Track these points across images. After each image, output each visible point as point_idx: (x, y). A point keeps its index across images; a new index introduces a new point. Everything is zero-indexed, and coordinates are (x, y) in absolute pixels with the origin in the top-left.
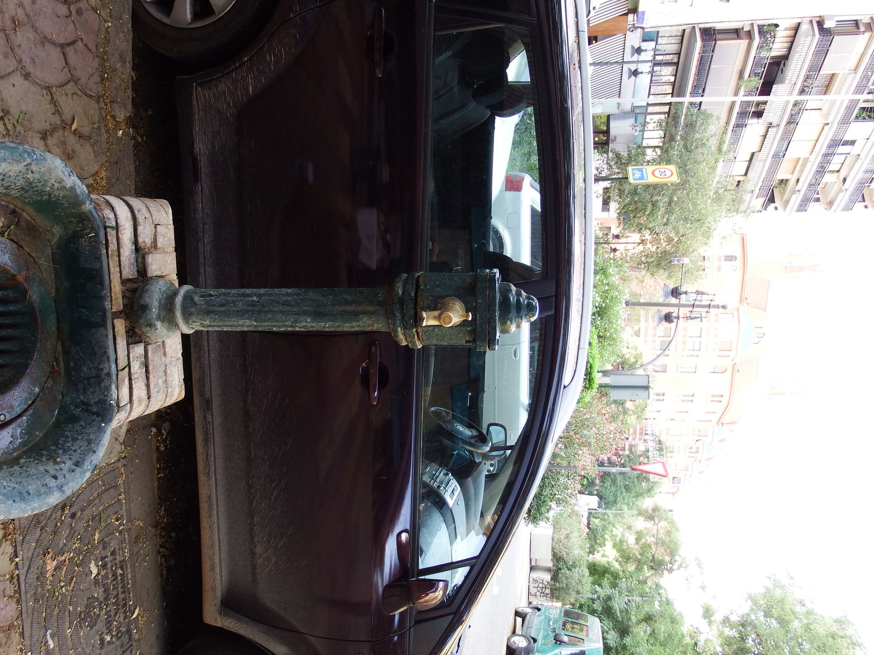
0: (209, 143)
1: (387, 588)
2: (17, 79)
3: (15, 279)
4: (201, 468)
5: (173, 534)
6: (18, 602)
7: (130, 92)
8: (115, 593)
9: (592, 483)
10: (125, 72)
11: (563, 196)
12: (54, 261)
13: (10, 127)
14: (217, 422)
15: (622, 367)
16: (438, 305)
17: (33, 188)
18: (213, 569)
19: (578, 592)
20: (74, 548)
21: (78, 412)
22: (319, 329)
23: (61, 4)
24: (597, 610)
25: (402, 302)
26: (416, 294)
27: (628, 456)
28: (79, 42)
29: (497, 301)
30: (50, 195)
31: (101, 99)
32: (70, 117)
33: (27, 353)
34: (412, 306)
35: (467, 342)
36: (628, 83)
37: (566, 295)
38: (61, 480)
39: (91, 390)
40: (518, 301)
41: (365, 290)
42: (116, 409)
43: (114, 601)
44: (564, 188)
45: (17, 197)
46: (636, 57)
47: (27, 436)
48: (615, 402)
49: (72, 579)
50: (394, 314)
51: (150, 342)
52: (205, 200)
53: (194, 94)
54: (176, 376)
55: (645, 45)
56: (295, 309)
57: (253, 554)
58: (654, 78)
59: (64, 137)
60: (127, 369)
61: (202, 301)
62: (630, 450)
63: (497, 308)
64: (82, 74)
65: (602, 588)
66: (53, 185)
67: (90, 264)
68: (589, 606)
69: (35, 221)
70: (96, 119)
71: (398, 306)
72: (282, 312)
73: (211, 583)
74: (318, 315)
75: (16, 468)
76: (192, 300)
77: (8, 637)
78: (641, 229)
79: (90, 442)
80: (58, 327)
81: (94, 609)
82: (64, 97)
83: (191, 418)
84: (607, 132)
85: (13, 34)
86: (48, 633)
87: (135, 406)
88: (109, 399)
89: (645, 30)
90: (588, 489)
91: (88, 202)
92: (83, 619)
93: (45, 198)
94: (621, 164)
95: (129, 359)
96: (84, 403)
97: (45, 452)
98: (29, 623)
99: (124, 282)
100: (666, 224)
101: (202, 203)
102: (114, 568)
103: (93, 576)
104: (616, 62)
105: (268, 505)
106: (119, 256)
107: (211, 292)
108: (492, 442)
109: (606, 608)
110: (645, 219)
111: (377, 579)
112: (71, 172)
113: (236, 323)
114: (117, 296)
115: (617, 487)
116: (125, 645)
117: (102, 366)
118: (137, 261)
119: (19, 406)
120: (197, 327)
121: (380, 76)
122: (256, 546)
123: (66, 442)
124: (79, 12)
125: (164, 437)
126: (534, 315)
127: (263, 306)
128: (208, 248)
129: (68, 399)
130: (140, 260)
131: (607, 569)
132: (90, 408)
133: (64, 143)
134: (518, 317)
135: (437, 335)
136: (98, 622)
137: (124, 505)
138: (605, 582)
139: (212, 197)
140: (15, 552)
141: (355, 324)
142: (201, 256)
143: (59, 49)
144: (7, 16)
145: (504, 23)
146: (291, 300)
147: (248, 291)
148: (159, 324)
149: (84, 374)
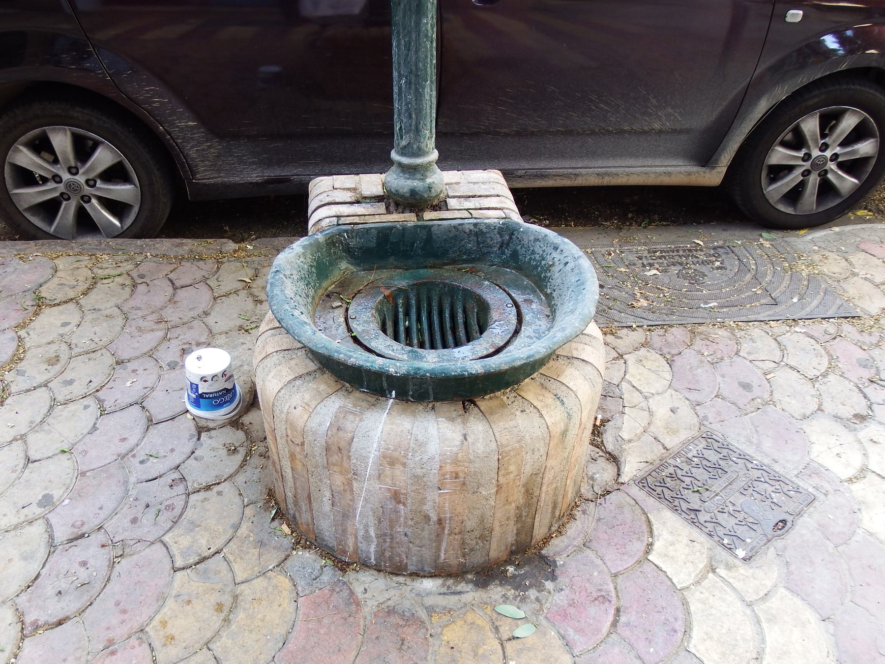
0: (251, 167)
2: (210, 320)
3: (388, 296)
4: (569, 182)
5: (630, 215)
6: (671, 326)
8: (677, 258)
10: (189, 245)
12: (371, 269)
14: (525, 165)
20: (630, 287)
21: (508, 252)
22: (434, 10)
23: (137, 289)
30: (311, 266)
32: (240, 283)
33: (453, 291)
38: (568, 259)
39: (489, 241)
45: (315, 292)
49: (659, 289)
53: (204, 181)
54: (479, 175)
56: (414, 36)
57: (660, 132)
60: (470, 211)
61: (406, 137)
64: (199, 275)
66: (302, 262)
67: (372, 238)
72: (417, 51)
73: (682, 176)
75: (554, 295)
76: (405, 147)
77: (700, 333)
79: (537, 240)
80: (431, 267)
85: (171, 323)
87: (505, 206)
88: (499, 225)
92: (696, 282)
93: (313, 269)
95: (461, 210)
96: (501, 247)
98: (692, 319)
99: (388, 211)
101: (310, 175)
103: (658, 273)
105: (613, 114)
106: (365, 215)
107: (398, 129)
113: (428, 103)
114: (402, 217)
117: (467, 231)
120: (431, 143)
122: (653, 129)
123: (535, 260)
124: (142, 276)
127: (411, 72)
137: (596, 249)
139: (303, 165)
140: (627, 327)
143: (178, 291)
144: (155, 327)
147: (396, 89)
148: (429, 181)
149: (474, 246)
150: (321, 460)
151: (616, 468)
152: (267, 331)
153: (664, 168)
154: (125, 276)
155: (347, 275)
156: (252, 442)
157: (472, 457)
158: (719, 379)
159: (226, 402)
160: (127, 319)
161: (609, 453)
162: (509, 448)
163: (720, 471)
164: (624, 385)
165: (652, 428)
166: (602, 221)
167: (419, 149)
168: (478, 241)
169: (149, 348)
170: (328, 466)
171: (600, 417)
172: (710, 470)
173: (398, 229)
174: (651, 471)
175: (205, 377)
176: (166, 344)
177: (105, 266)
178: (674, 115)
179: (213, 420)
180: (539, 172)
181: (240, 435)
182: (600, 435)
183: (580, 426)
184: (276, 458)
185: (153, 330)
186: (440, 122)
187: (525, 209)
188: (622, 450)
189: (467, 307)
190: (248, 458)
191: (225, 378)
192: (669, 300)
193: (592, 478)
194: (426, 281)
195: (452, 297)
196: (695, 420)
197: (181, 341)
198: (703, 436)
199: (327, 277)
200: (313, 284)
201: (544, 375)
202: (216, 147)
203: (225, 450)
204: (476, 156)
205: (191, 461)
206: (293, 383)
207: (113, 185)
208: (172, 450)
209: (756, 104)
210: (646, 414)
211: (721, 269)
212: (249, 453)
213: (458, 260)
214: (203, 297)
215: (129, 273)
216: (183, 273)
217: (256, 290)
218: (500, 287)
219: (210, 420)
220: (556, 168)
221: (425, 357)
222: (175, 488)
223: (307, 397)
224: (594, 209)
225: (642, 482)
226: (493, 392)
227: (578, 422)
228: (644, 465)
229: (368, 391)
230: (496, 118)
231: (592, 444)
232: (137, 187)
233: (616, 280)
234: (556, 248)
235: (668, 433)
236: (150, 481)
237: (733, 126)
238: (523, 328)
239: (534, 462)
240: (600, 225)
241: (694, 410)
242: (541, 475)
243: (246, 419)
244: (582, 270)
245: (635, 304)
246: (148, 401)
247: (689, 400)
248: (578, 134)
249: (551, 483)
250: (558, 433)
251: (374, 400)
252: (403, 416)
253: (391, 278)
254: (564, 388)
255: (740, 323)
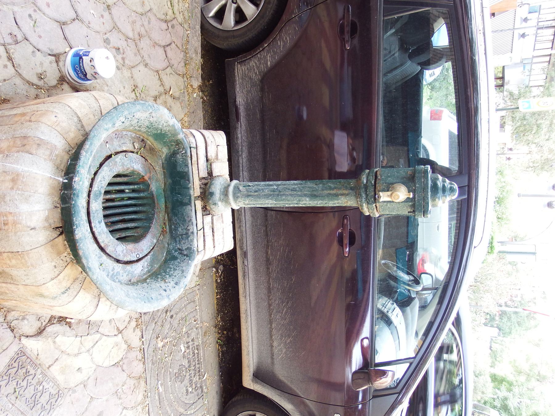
1: (353, 380)
2: (141, 67)
3: (144, 178)
5: (225, 332)
6: (144, 363)
7: (200, 70)
8: (194, 363)
9: (492, 319)
10: (197, 59)
11: (473, 121)
13: (138, 95)
15: (515, 240)
16: (389, 188)
17: (153, 126)
18: (248, 354)
19: (483, 393)
20: (172, 335)
21: (176, 254)
24: (497, 406)
25: (366, 187)
26: (375, 182)
27: (520, 302)
28: (173, 43)
29: (429, 186)
30: (161, 130)
31: (185, 76)
33: (149, 220)
34: (373, 190)
35: (409, 212)
36: (518, 42)
37: (475, 187)
40: (444, 186)
41: (342, 181)
42: (197, 253)
43: (193, 368)
44: (473, 113)
45: (144, 132)
46: (524, 25)
47: (150, 267)
48: (510, 263)
49: (171, 353)
50: (361, 195)
51: (214, 214)
52: (242, 132)
55: (530, 16)
56: (299, 193)
58: (537, 38)
59: (166, 99)
60: (202, 229)
61: (244, 189)
62: (522, 297)
63: (429, 190)
64: (174, 62)
65: (501, 391)
66: (163, 124)
68: (491, 403)
69: (153, 145)
70: (182, 87)
71: (363, 190)
72: (291, 195)
74: (313, 196)
75: (145, 284)
77: (139, 383)
78: (529, 143)
80: (166, 206)
81: (183, 372)
82: (165, 76)
83: (235, 263)
84: (503, 78)
86: (159, 383)
88: (193, 247)
89: (531, 6)
90: (490, 323)
91: (181, 133)
93: (159, 131)
94: (513, 99)
96: (180, 249)
97: (159, 276)
98: (149, 376)
99: (201, 179)
100: (548, 140)
102: (193, 349)
104: (509, 29)
106: (198, 164)
108: (423, 284)
109: (504, 405)
110: (532, 137)
111: (348, 373)
112: (173, 116)
113: (264, 202)
114: (197, 187)
115: (511, 322)
116: (199, 394)
117: (189, 228)
118: (207, 167)
119: (146, 250)
121: (348, 48)
123: (170, 271)
124: (173, 27)
125: (220, 274)
126: (454, 195)
127: (280, 192)
128: (245, 160)
129: (171, 247)
130: (209, 166)
131: (504, 378)
132: (183, 252)
133: (165, 102)
134: (444, 196)
135: (389, 208)
136: (185, 380)
137: (198, 312)
138: (503, 387)
140: (142, 335)
141: (336, 202)
142: (241, 165)
143: (163, 48)
144: (136, 32)
145: (431, 7)
146: (296, 188)
147: (271, 183)
148: (220, 203)
150: (18, 133)
151: (33, 334)
152: (117, 101)
153: (251, 351)
154: (173, 16)
155: (159, 153)
156: (48, 90)
157: (19, 233)
158: (105, 398)
159: (77, 74)
160: (142, 15)
161: (44, 329)
162: (27, 259)
163: (32, 405)
164: (98, 336)
165: (65, 357)
166: (221, 315)
167: (238, 197)
168: (183, 235)
169: (120, 27)
170: (14, 138)
171: (72, 321)
172: (33, 398)
173: (188, 184)
174: (31, 358)
175: (93, 61)
176: (123, 38)
177: (180, 4)
178: (281, 354)
179: (65, 65)
180: (247, 274)
181: (54, 82)
182: (58, 322)
183: (51, 306)
184: (27, 104)
185: (133, 30)
186: (273, 212)
187: (228, 267)
188: (47, 338)
189: (139, 229)
190: (35, 87)
191: (93, 74)
192: (163, 361)
193: (23, 319)
194: (156, 203)
195: (145, 219)
196: (72, 385)
197: (126, 48)
198: (60, 391)
199: (156, 140)
200: (149, 130)
201: (85, 280)
202: (256, 78)
203: (40, 72)
204: (254, 235)
205: (31, 49)
206: (75, 116)
207: (234, 14)
208: (40, 37)
209: (289, 402)
210: (76, 351)
211: (186, 392)
212: (38, 87)
213: (171, 223)
214: (160, 64)
215: (175, 19)
216: (176, 52)
217: (164, 97)
218: (152, 250)
219: (65, 63)
220: (249, 285)
221: (96, 201)
222: (10, 36)
223: (64, 125)
224: (229, 309)
225: (22, 353)
226: (69, 246)
227: (51, 304)
228: (36, 353)
229: (68, 164)
230: (276, 246)
231: (52, 317)
232: (232, 28)
233: (176, 326)
234: (176, 284)
235: (62, 367)
236: (15, 20)
237: (277, 390)
238: (121, 265)
239: (19, 276)
240: (218, 314)
241: (81, 384)
242: (12, 282)
243: (66, 86)
244: (159, 300)
245: (159, 339)
246: (79, 23)
247: (88, 379)
248: (269, 297)
249: (8, 290)
250: (41, 291)
251: (62, 168)
252: (49, 187)
253: (157, 180)
254: (75, 293)
255: (147, 408)
